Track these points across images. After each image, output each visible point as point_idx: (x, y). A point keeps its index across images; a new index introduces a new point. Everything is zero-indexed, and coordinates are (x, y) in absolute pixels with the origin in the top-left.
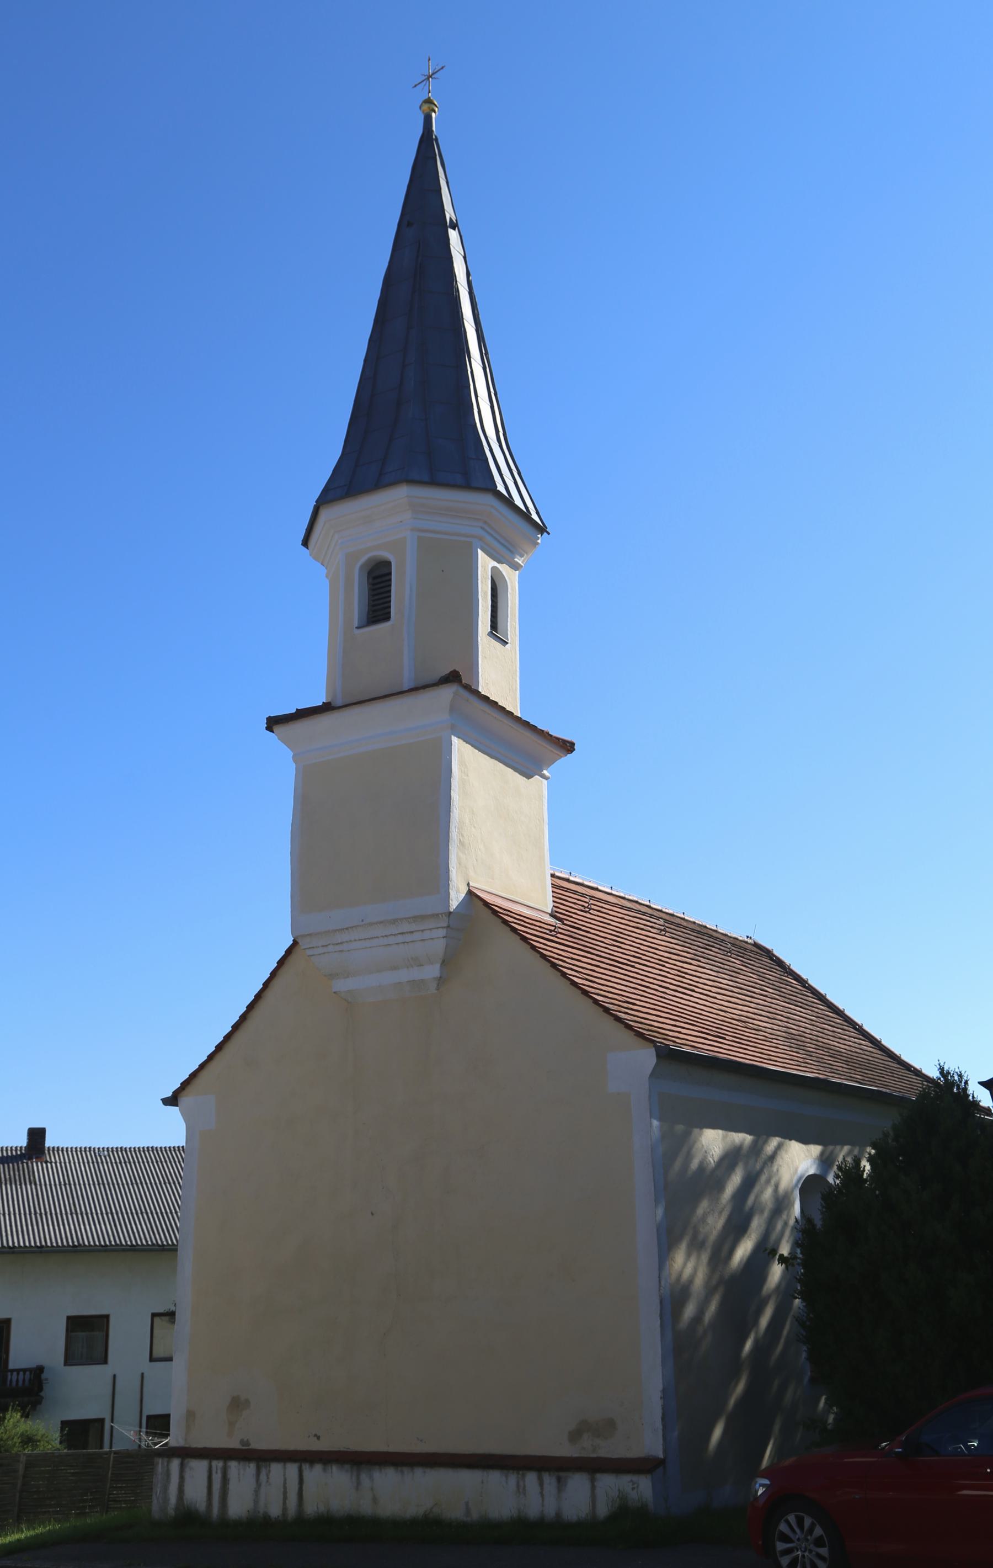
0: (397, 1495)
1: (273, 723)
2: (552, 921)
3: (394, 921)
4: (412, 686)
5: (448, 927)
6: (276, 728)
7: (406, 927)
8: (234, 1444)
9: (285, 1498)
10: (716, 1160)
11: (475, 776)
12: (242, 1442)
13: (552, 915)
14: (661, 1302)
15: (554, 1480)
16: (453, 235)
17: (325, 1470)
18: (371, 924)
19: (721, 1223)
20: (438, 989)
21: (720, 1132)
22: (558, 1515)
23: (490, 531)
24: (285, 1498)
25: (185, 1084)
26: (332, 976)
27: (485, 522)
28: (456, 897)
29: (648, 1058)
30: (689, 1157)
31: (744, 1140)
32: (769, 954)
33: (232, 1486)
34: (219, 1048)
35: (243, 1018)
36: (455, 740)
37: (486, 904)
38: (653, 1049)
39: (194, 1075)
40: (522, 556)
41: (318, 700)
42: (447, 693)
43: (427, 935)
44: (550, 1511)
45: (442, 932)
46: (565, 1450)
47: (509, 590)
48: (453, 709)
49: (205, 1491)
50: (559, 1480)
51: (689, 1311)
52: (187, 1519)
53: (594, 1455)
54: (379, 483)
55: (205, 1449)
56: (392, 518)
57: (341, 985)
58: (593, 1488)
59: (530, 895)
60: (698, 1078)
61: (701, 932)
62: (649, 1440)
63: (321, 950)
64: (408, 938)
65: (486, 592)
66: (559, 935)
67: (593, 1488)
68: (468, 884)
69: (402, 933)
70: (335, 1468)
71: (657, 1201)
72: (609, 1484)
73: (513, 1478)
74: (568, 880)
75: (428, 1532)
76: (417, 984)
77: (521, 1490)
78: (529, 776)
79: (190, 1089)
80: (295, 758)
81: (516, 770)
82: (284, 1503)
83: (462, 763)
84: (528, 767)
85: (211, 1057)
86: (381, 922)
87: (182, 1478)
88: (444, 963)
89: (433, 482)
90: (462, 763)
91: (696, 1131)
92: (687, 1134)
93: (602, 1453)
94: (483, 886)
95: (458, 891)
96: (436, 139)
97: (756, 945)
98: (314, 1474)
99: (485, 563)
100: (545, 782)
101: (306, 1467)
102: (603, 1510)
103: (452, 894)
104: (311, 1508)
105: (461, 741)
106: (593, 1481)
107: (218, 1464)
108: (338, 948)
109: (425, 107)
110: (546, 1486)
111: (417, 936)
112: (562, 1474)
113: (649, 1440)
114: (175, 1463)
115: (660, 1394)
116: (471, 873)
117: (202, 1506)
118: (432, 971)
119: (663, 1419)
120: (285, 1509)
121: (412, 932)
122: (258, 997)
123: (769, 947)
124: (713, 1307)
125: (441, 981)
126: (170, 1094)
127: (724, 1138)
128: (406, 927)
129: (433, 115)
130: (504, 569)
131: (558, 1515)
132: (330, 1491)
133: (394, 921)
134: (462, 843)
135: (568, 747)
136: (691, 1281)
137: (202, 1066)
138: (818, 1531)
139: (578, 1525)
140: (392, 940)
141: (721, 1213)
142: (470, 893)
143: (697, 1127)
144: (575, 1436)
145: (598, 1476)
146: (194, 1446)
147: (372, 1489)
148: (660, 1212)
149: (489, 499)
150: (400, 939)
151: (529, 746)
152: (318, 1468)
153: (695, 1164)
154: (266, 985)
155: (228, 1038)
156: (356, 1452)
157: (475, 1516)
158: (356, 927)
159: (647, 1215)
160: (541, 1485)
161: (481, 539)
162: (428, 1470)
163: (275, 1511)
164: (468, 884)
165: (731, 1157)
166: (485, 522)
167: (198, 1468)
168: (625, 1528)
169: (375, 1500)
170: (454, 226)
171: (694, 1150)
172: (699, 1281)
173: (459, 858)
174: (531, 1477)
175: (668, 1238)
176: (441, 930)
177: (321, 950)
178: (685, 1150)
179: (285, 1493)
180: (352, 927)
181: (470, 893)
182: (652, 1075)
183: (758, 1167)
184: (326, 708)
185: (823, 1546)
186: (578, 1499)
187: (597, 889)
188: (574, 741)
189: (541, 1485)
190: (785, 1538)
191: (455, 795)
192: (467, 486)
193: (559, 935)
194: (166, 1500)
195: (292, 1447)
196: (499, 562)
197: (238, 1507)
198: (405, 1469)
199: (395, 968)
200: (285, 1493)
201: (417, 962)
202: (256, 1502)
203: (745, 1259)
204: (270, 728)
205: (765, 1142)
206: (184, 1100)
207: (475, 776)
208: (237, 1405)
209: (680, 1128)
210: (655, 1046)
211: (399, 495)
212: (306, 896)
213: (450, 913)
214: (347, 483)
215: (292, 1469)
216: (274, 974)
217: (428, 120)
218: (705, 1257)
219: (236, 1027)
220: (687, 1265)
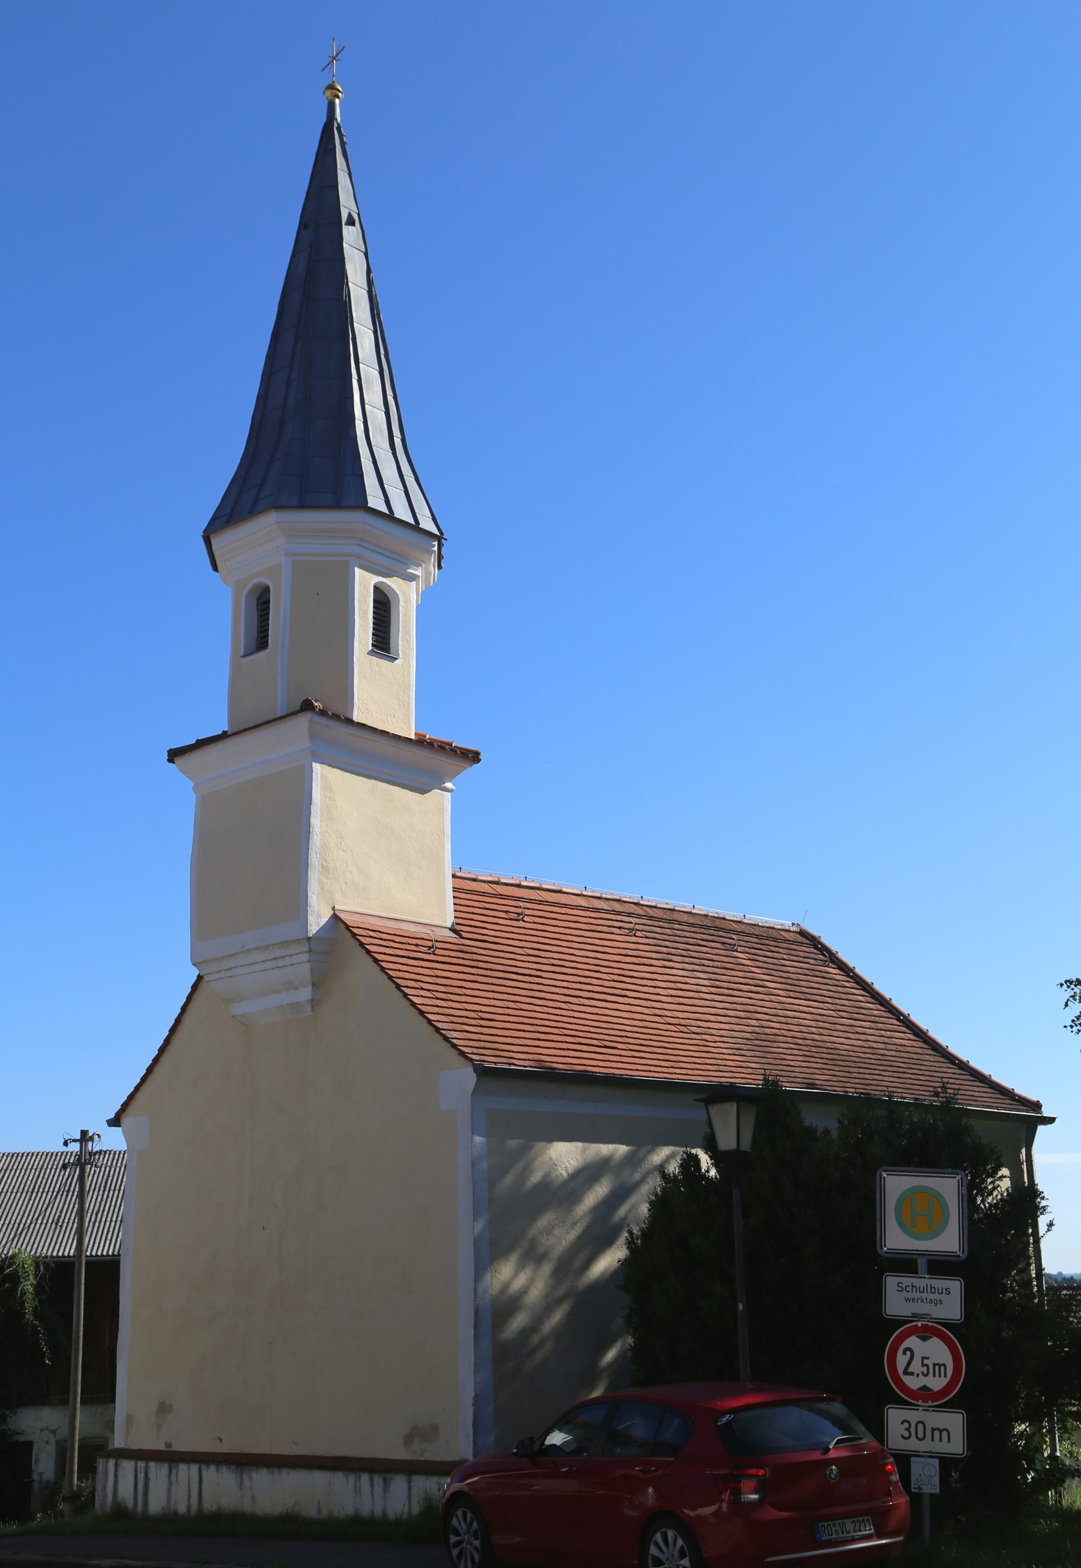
0: (271, 1494)
1: (174, 755)
3: (267, 947)
5: (310, 951)
7: (278, 953)
8: (161, 1447)
9: (189, 1497)
11: (341, 802)
12: (168, 1445)
13: (452, 930)
14: (476, 1313)
15: (381, 1481)
16: (350, 236)
17: (217, 1470)
18: (249, 951)
19: (573, 1235)
21: (580, 1144)
22: (384, 1514)
23: (371, 547)
24: (189, 1497)
25: (125, 1106)
26: (229, 1001)
27: (361, 540)
28: (317, 919)
29: (469, 1077)
30: (527, 1171)
32: (814, 942)
33: (152, 1484)
34: (150, 1070)
36: (317, 767)
39: (131, 1097)
40: (418, 565)
41: (220, 725)
42: (303, 721)
43: (295, 959)
44: (378, 1511)
45: (306, 957)
46: (400, 1453)
47: (401, 603)
48: (312, 736)
49: (132, 1488)
50: (385, 1480)
51: (519, 1321)
52: (119, 1512)
53: (422, 1459)
54: (253, 512)
55: (139, 1450)
56: (269, 542)
57: (237, 1009)
58: (410, 1488)
59: (432, 909)
60: (533, 1092)
61: (715, 929)
62: (460, 1445)
63: (215, 976)
64: (281, 963)
65: (365, 612)
66: (438, 952)
67: (410, 1488)
68: (333, 908)
70: (224, 1469)
71: (476, 1216)
72: (425, 1485)
73: (352, 1479)
74: (519, 886)
75: (287, 1528)
76: (296, 1006)
77: (357, 1490)
78: (423, 791)
79: (128, 1111)
82: (189, 1501)
83: (327, 787)
84: (421, 783)
85: (144, 1080)
86: (257, 948)
87: (116, 1476)
89: (303, 505)
90: (327, 787)
92: (523, 1151)
93: (429, 1457)
94: (351, 906)
95: (319, 916)
97: (803, 933)
98: (210, 1473)
99: (364, 583)
100: (449, 794)
101: (204, 1467)
102: (416, 1510)
103: (311, 919)
104: (209, 1505)
105: (325, 766)
106: (409, 1482)
107: (141, 1464)
108: (228, 974)
110: (376, 1487)
112: (387, 1476)
113: (460, 1445)
114: (112, 1463)
115: (472, 1401)
116: (338, 896)
117: (130, 1504)
118: (305, 994)
119: (474, 1424)
120: (189, 1507)
122: (178, 1020)
123: (816, 933)
124: (557, 1317)
125: (314, 1003)
126: (112, 1116)
127: (584, 1150)
128: (278, 953)
129: (337, 101)
130: (394, 584)
131: (384, 1514)
132: (222, 1490)
133: (267, 947)
135: (473, 757)
136: (524, 1291)
138: (475, 1526)
139: (398, 1522)
140: (269, 965)
141: (574, 1224)
142: (335, 918)
143: (543, 1140)
144: (408, 1440)
145: (414, 1477)
146: (132, 1447)
147: (251, 1489)
148: (480, 1225)
149: (359, 516)
150: (274, 963)
152: (213, 1468)
153: (535, 1178)
155: (156, 1061)
156: (248, 1454)
157: (325, 1513)
159: (467, 1229)
160: (372, 1485)
161: (358, 557)
162: (291, 1471)
163: (182, 1509)
164: (333, 908)
165: (589, 1173)
167: (128, 1466)
168: (429, 1527)
169: (253, 1498)
170: (351, 222)
171: (537, 1162)
172: (536, 1292)
173: (320, 882)
174: (365, 1477)
175: (489, 1252)
177: (215, 976)
178: (521, 1165)
179: (189, 1491)
181: (335, 918)
182: (475, 1092)
183: (637, 1176)
184: (224, 735)
185: (477, 1538)
186: (399, 1499)
187: (560, 892)
189: (372, 1485)
190: (457, 1533)
191: (316, 821)
193: (438, 952)
194: (105, 1497)
195: (339, 1453)
197: (156, 1504)
198: (275, 1470)
199: (277, 991)
200: (189, 1491)
201: (291, 986)
202: (169, 1500)
203: (612, 1269)
204: (171, 760)
206: (125, 1120)
207: (341, 802)
208: (164, 1409)
209: (513, 1143)
210: (473, 1064)
212: (203, 926)
213: (309, 939)
214: (233, 511)
215: (194, 1468)
218: (547, 1268)
220: (506, 1275)
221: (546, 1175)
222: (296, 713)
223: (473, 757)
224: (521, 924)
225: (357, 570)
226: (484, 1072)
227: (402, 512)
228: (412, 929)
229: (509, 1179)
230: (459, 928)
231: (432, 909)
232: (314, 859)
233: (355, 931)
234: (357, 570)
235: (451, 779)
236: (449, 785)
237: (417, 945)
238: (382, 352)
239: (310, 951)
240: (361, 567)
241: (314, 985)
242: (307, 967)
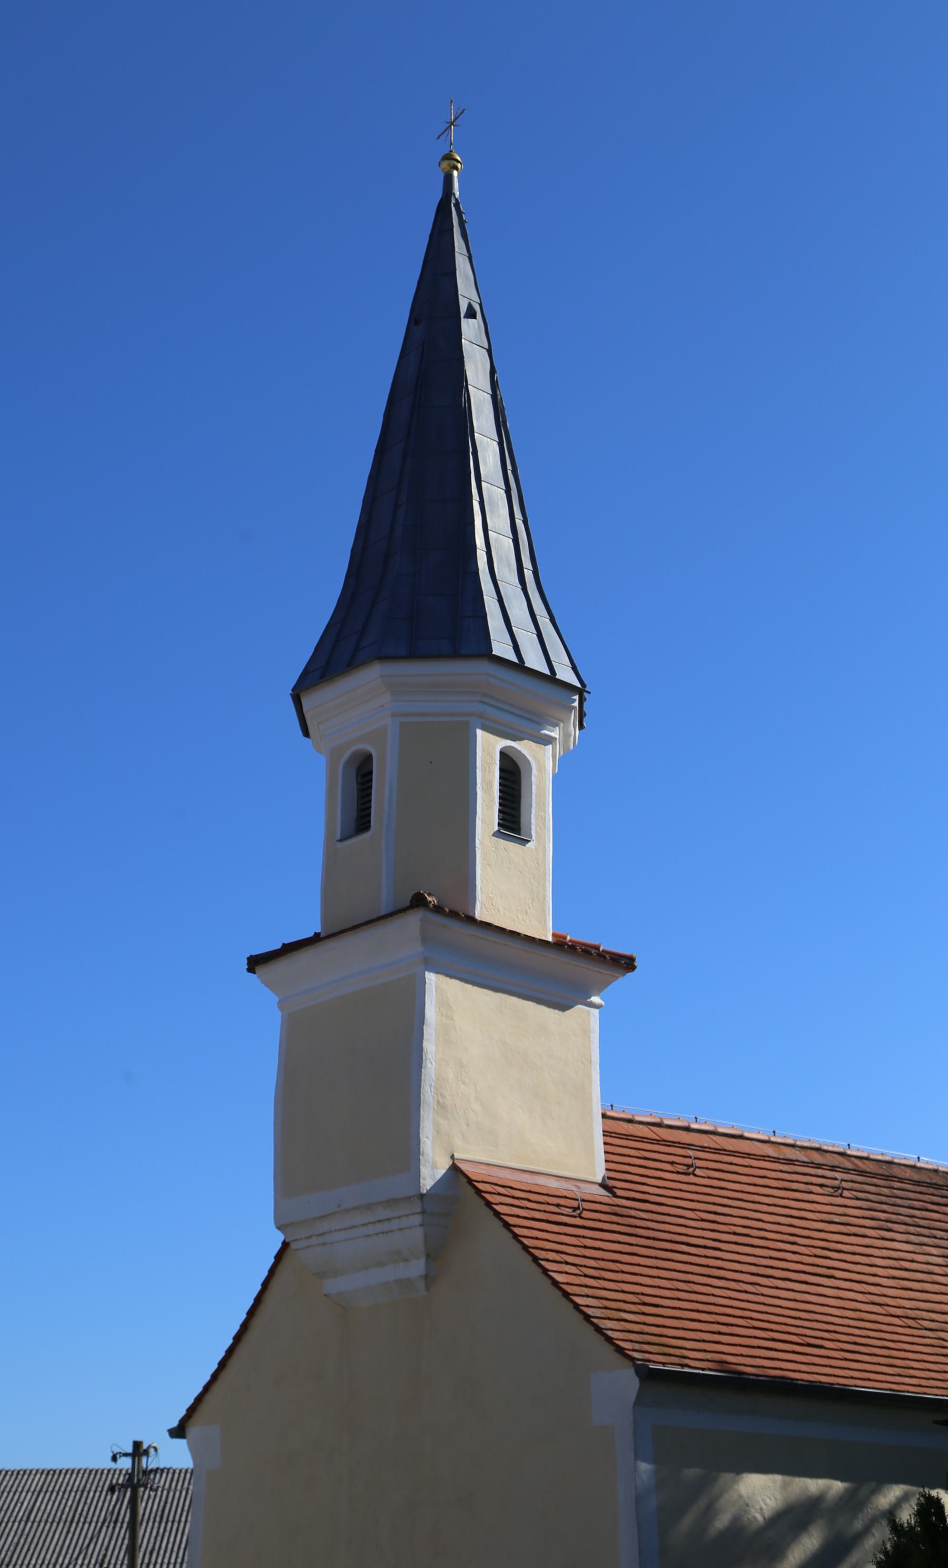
2: (602, 1191)
3: (369, 1207)
4: (390, 909)
6: (257, 969)
10: (767, 1514)
11: (459, 1018)
13: (603, 1185)
18: (347, 1211)
20: (427, 1289)
21: (778, 1478)
25: (192, 1410)
27: (485, 695)
28: (431, 1173)
30: (710, 1512)
31: (830, 1488)
34: (223, 1364)
35: (245, 1327)
37: (470, 1181)
38: (633, 1370)
39: (199, 1399)
41: (311, 926)
42: (414, 920)
47: (534, 772)
56: (370, 701)
57: (334, 1286)
59: (580, 1161)
64: (386, 1227)
68: (452, 1157)
69: (379, 1221)
74: (687, 1129)
76: (405, 1284)
78: (563, 1007)
79: (197, 1417)
80: (281, 1005)
81: (539, 1001)
83: (443, 1004)
84: (561, 998)
85: (215, 1376)
88: (430, 1256)
89: (413, 654)
91: (727, 1477)
94: (476, 1154)
95: (434, 1167)
96: (457, 205)
99: (488, 748)
100: (596, 1012)
103: (425, 1171)
105: (441, 977)
109: (445, 164)
111: (394, 1224)
118: (417, 1267)
121: (389, 1220)
122: (258, 1300)
125: (429, 1279)
126: (175, 1424)
127: (785, 1486)
128: (383, 1213)
129: (455, 173)
133: (369, 1207)
134: (441, 1106)
135: (626, 964)
137: (207, 1388)
140: (371, 1229)
143: (729, 1470)
149: (481, 667)
150: (379, 1227)
151: (565, 968)
153: (722, 1521)
154: (266, 1285)
155: (230, 1352)
158: (334, 1213)
161: (480, 716)
164: (452, 1157)
166: (485, 695)
170: (471, 314)
171: (722, 1502)
176: (417, 1216)
178: (702, 1503)
180: (330, 1214)
182: (638, 1402)
183: (858, 1525)
184: (316, 939)
187: (741, 1137)
188: (634, 955)
191: (430, 1046)
192: (455, 654)
196: (514, 739)
205: (876, 1491)
206: (192, 1430)
207: (459, 1018)
209: (691, 1473)
211: (371, 676)
213: (422, 1196)
214: (331, 660)
216: (272, 1271)
217: (448, 179)
219: (238, 1338)
221: (736, 1520)
222: (404, 910)
223: (626, 964)
224: (691, 1179)
225: (479, 733)
226: (647, 1375)
227: (534, 660)
228: (552, 1184)
229: (687, 1522)
230: (611, 1183)
231: (580, 1161)
232: (428, 1093)
233: (480, 1186)
234: (479, 733)
235: (598, 992)
236: (595, 999)
237: (558, 1205)
238: (509, 467)
239: (423, 1212)
240: (484, 728)
241: (428, 1256)
242: (418, 1234)
